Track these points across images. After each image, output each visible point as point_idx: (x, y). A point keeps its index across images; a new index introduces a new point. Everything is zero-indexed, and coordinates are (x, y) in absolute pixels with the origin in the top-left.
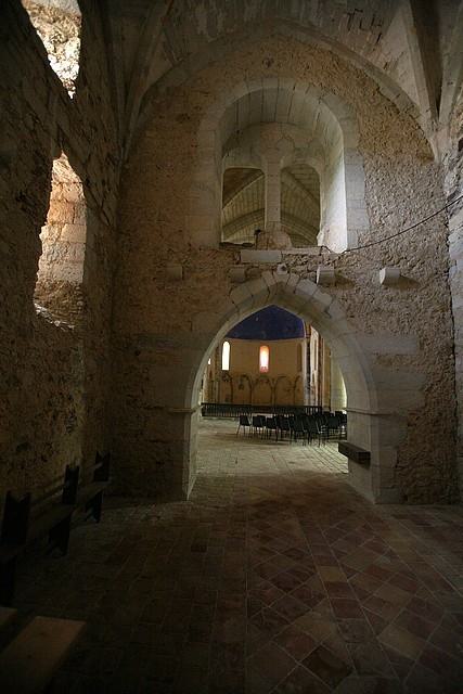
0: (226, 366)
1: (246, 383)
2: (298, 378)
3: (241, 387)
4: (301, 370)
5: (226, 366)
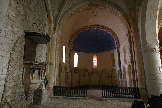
0: (76, 65)
1: (87, 74)
2: (113, 70)
3: (84, 76)
4: (114, 65)
5: (76, 65)
